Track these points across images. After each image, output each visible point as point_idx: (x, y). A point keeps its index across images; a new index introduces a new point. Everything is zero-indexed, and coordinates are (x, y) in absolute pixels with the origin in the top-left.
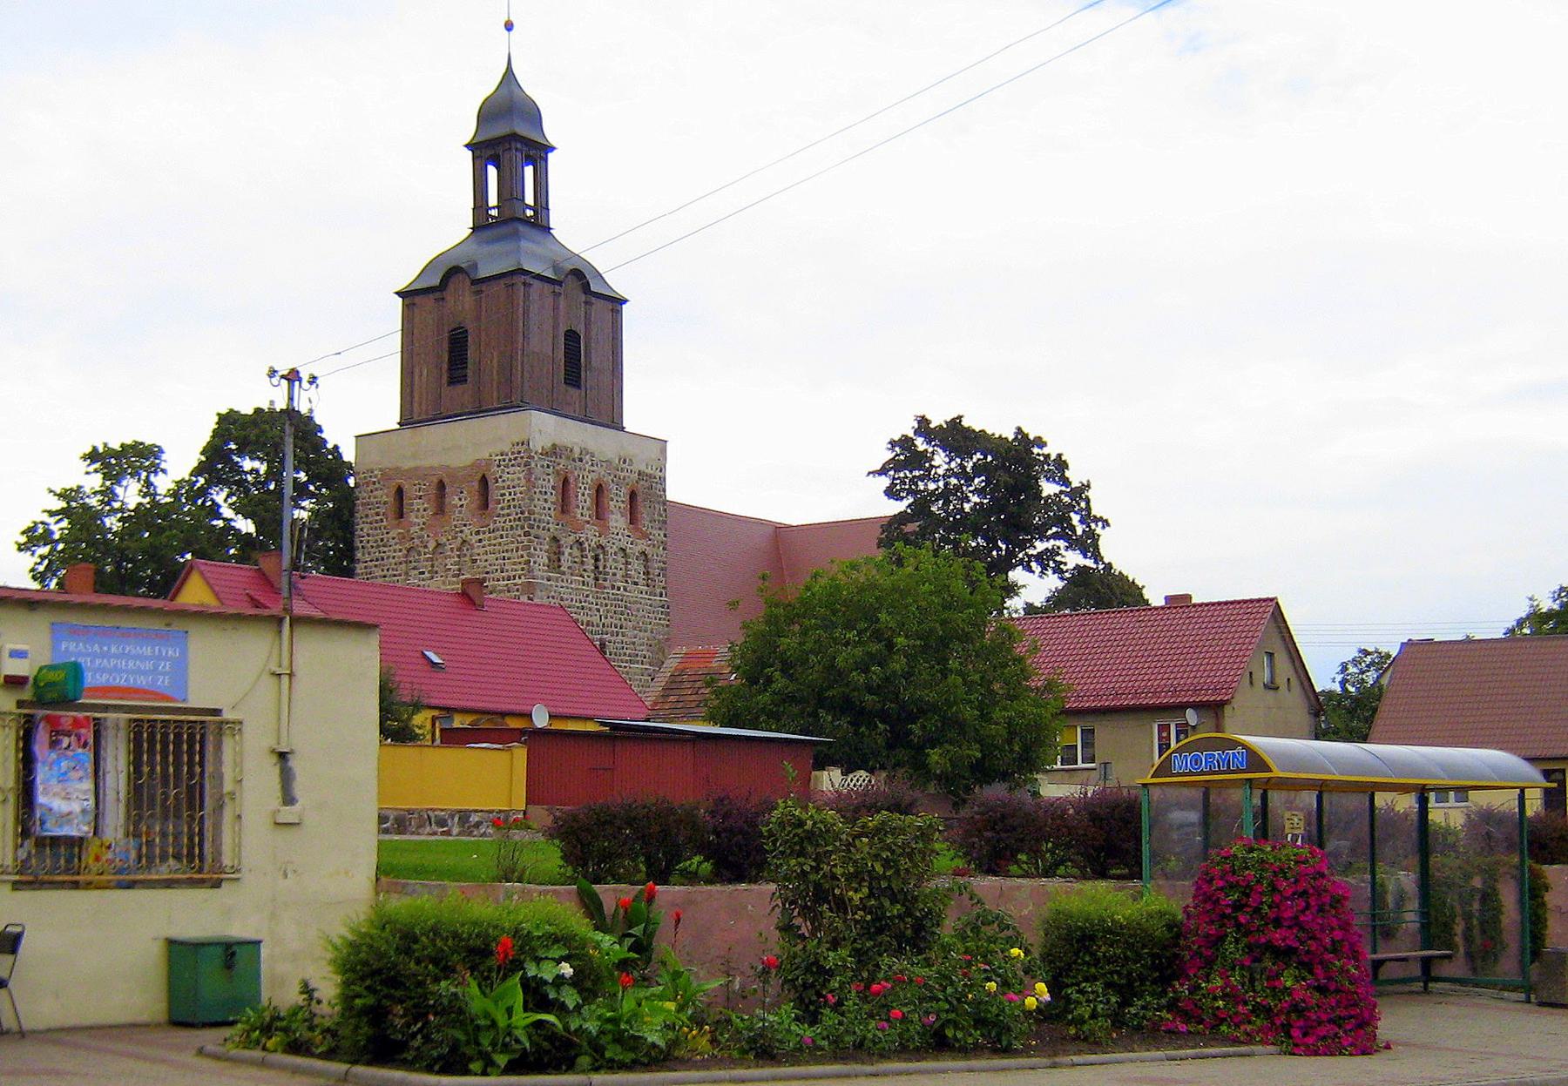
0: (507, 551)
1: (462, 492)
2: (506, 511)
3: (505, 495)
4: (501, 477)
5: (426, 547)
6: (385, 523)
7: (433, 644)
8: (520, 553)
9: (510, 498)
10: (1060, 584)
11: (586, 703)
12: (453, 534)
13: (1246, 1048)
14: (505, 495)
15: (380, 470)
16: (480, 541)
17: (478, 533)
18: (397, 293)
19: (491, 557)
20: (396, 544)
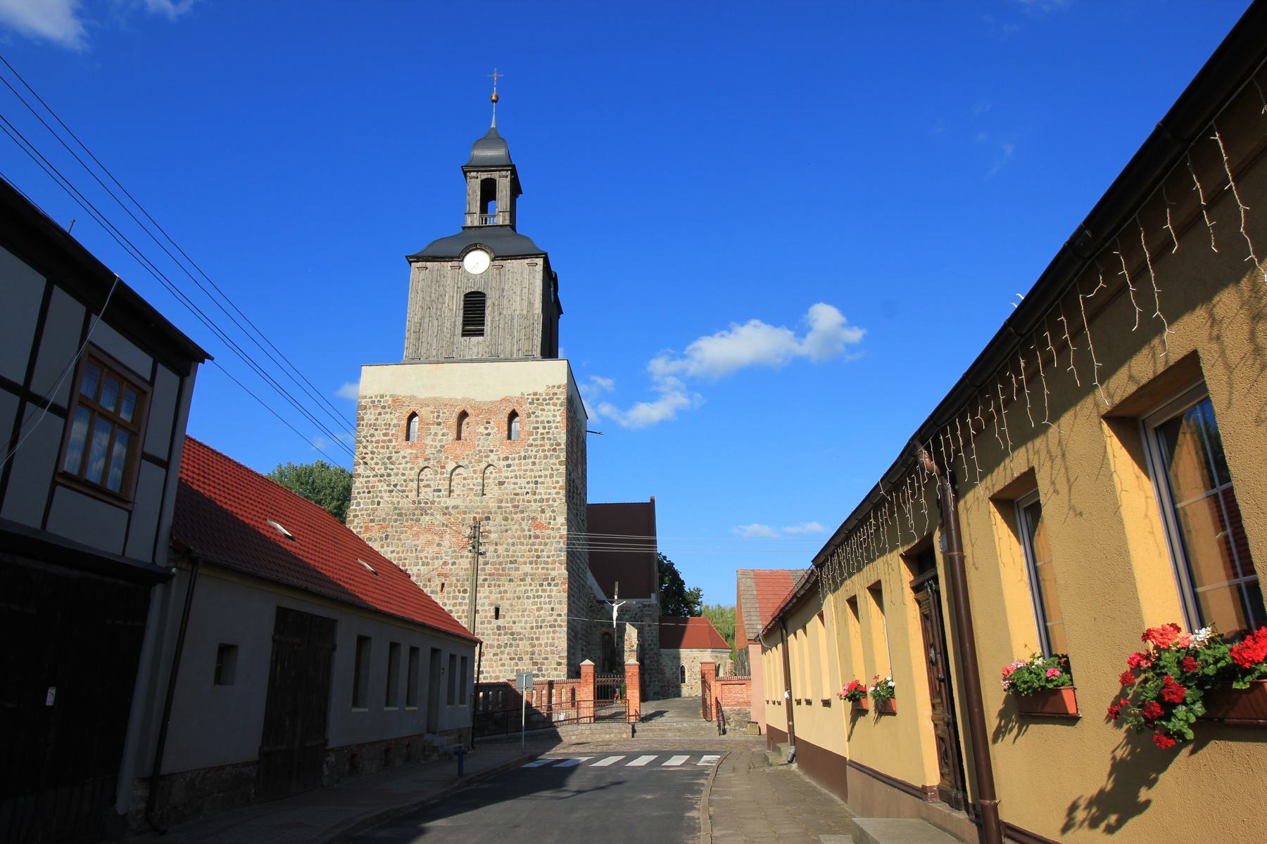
0: (540, 476)
1: (489, 423)
2: (539, 442)
3: (538, 428)
4: (534, 413)
5: (443, 467)
6: (394, 443)
7: (284, 521)
8: (555, 479)
9: (544, 431)
10: (553, 720)
11: (318, 530)
12: (477, 457)
13: (955, 748)
14: (538, 428)
15: (391, 396)
16: (509, 466)
17: (507, 458)
18: (767, 725)
19: (522, 482)
20: (406, 463)
